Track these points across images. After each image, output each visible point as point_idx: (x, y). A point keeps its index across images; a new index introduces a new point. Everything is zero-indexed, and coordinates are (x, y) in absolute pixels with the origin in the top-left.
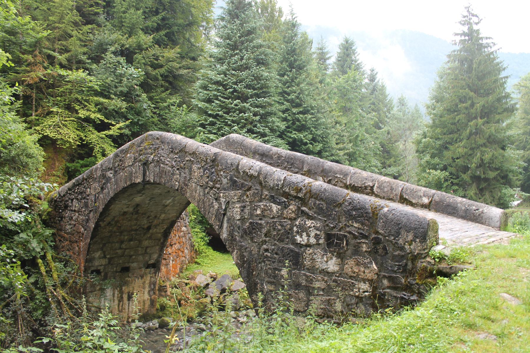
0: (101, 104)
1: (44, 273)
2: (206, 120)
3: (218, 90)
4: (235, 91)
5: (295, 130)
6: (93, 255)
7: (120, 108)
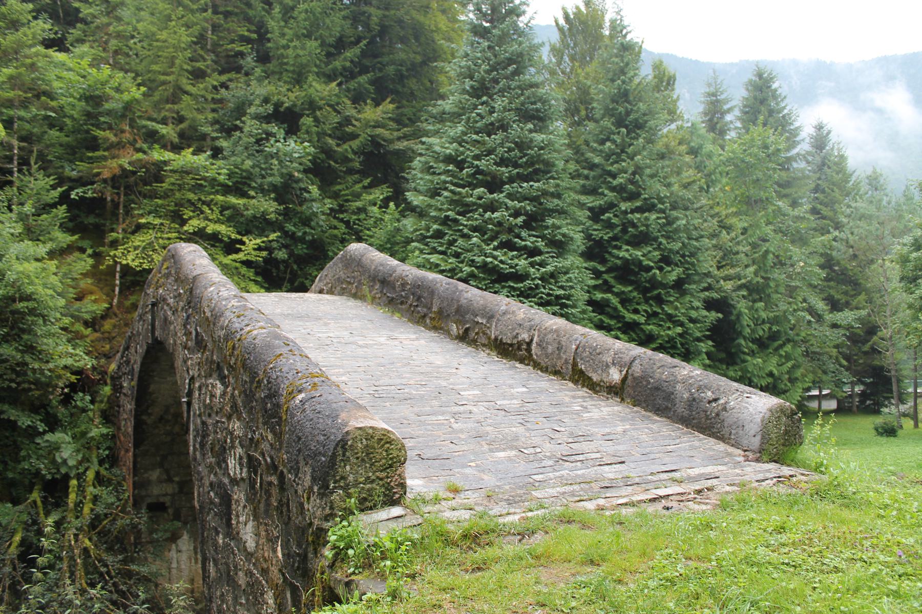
0: (233, 207)
1: (71, 505)
2: (428, 229)
3: (446, 172)
4: (479, 171)
5: (628, 243)
6: (146, 475)
7: (264, 214)
